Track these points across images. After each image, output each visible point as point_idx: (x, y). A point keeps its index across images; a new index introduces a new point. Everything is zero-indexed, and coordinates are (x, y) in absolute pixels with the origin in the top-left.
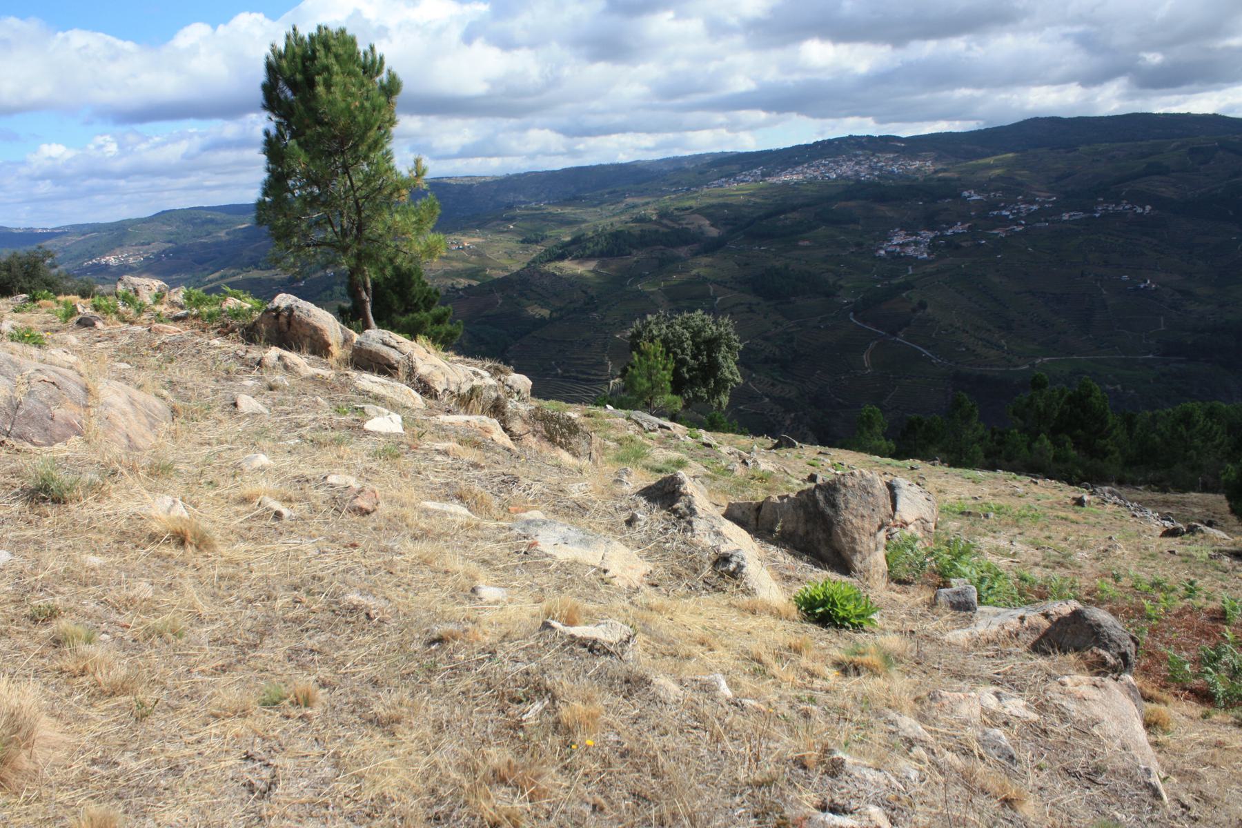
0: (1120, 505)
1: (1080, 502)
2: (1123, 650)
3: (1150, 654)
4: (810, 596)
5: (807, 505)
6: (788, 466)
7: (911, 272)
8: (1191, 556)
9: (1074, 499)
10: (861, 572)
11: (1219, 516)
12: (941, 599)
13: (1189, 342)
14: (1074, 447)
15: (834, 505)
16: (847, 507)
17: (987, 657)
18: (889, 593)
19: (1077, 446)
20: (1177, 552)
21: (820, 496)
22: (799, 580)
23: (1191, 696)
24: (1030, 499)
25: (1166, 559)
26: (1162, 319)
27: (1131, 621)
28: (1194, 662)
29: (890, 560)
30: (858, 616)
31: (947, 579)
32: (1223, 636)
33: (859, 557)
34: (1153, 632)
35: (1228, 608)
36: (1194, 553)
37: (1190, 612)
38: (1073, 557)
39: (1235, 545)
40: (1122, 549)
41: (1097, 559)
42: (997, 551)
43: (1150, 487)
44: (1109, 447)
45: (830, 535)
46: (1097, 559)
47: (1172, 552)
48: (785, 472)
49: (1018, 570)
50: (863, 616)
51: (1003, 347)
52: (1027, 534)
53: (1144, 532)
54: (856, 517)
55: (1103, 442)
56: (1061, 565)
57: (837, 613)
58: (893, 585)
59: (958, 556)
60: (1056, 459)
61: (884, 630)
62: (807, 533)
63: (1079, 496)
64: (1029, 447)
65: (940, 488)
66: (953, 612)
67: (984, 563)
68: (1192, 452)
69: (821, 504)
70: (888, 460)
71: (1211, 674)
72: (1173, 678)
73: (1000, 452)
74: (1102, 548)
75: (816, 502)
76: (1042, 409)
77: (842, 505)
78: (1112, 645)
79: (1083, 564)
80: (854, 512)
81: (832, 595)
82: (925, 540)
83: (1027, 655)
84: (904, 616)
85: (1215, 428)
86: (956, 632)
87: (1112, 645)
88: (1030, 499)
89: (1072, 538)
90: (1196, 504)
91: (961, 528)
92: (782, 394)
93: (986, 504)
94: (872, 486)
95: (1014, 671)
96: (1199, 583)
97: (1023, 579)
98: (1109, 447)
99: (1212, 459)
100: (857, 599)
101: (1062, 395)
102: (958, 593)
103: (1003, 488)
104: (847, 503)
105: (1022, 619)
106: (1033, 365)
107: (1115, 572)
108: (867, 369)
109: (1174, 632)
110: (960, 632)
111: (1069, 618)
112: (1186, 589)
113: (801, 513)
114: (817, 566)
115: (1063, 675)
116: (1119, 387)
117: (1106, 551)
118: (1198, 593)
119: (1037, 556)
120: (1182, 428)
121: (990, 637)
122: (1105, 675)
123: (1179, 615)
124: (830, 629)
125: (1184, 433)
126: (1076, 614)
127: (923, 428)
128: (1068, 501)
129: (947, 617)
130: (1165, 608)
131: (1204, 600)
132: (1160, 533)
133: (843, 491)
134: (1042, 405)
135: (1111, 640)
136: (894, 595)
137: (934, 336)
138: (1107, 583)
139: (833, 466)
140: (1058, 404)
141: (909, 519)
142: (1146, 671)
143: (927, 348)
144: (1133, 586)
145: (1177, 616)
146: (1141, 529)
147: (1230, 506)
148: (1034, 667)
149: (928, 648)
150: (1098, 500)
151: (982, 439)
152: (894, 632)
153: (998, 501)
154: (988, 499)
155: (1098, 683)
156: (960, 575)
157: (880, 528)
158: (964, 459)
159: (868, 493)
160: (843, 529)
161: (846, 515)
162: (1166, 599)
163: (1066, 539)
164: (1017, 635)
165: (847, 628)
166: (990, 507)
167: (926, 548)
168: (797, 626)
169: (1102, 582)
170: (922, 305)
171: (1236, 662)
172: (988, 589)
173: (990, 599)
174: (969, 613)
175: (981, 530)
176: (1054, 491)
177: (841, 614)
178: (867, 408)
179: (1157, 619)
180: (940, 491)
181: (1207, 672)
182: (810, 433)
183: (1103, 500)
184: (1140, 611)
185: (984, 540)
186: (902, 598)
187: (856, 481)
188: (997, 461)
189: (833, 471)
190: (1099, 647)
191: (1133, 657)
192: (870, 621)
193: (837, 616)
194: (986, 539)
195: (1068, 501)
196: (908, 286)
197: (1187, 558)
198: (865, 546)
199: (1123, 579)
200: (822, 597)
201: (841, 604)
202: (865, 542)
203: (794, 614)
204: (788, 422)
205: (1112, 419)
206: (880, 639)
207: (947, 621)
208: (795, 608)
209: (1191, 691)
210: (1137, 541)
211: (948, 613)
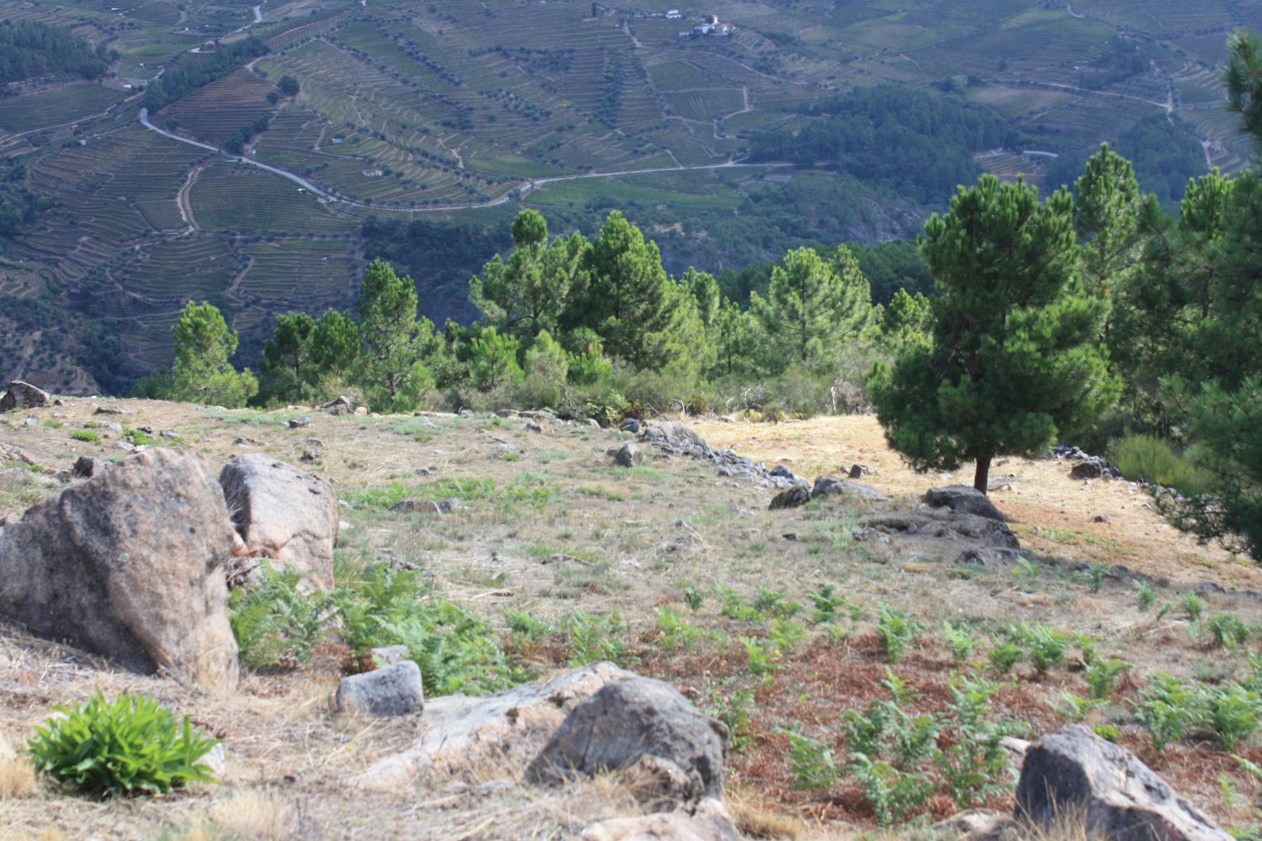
0: (695, 457)
1: (622, 458)
2: (699, 753)
3: (762, 742)
4: (63, 736)
5: (48, 536)
6: (32, 447)
7: (259, 19)
8: (823, 540)
9: (610, 453)
10: (179, 664)
11: (868, 456)
12: (350, 697)
13: (796, 134)
14: (605, 351)
15: (106, 530)
16: (134, 533)
17: (443, 808)
18: (243, 700)
19: (609, 350)
20: (798, 534)
21: (73, 515)
22: (45, 701)
23: (836, 810)
24: (528, 464)
25: (781, 551)
26: (745, 91)
27: (726, 682)
28: (840, 743)
29: (241, 629)
30: (169, 765)
31: (365, 651)
32: (884, 686)
33: (172, 633)
34: (763, 697)
35: (889, 633)
36: (828, 534)
37: (827, 648)
38: (612, 571)
39: (895, 508)
40: (703, 544)
41: (657, 568)
42: (468, 578)
43: (747, 414)
44: (668, 345)
45: (105, 593)
46: (657, 568)
47: (790, 537)
48: (25, 460)
49: (509, 611)
50: (181, 762)
51: (455, 163)
52: (524, 533)
53: (742, 502)
54: (156, 549)
55: (657, 336)
56: (590, 587)
57: (124, 765)
58: (254, 680)
59: (382, 603)
60: (573, 376)
61: (229, 784)
62: (55, 596)
63: (617, 446)
64: (521, 360)
65: (351, 459)
66: (377, 721)
67: (441, 605)
68: (814, 341)
69: (79, 531)
70: (243, 412)
71: (865, 765)
72: (804, 783)
73: (466, 374)
74: (665, 545)
75: (67, 528)
76: (538, 283)
77: (125, 529)
78: (678, 746)
79: (631, 581)
80: (152, 540)
81: (109, 729)
82: (315, 577)
83: (523, 791)
84: (278, 744)
85: (850, 292)
86: (385, 761)
87: (678, 746)
88: (528, 464)
89: (609, 533)
90: (829, 438)
91: (394, 537)
92: (11, 293)
93: (444, 480)
94: (185, 481)
95: (497, 830)
96: (838, 589)
97: (520, 627)
98: (668, 345)
99: (850, 350)
100: (164, 729)
101: (573, 253)
102: (382, 681)
103: (475, 446)
104: (133, 525)
105: (512, 715)
106: (516, 196)
107: (690, 591)
108: (186, 226)
109: (801, 692)
110: (394, 760)
111: (594, 706)
112: (818, 606)
113: (38, 555)
114: (82, 663)
115: (590, 822)
116: (678, 227)
117: (674, 549)
118: (838, 610)
119: (544, 577)
120: (793, 298)
121: (454, 763)
122: (671, 807)
123: (808, 657)
124: (112, 802)
125: (798, 303)
126: (608, 696)
127: (310, 339)
128: (600, 457)
129: (366, 732)
130: (782, 648)
131: (849, 622)
132: (768, 501)
133: (124, 497)
134: (537, 273)
135: (675, 738)
136: (256, 702)
137: (317, 148)
138: (677, 614)
139: (129, 436)
140: (567, 270)
141: (278, 536)
142: (756, 776)
143: (306, 175)
144: (724, 613)
145: (805, 659)
146: (736, 497)
147: (887, 435)
148: (532, 817)
149: (323, 810)
150: (654, 451)
151: (429, 349)
152: (253, 785)
153: (468, 473)
154: (449, 471)
155: (657, 828)
156: (389, 639)
157: (211, 566)
158: (398, 396)
159: (178, 495)
160: (131, 578)
161: (131, 548)
162: (783, 630)
163: (597, 536)
164: (506, 747)
165: (149, 794)
166: (453, 487)
167: (317, 593)
168: (39, 809)
169: (668, 611)
170: (289, 87)
171: (906, 733)
172: (446, 661)
173: (453, 680)
174: (410, 717)
175: (431, 537)
176: (573, 442)
177: (133, 765)
178: (192, 310)
179: (771, 671)
180: (354, 466)
181: (858, 762)
182: (79, 370)
183: (664, 449)
184: (740, 658)
185: (438, 558)
186: (272, 705)
187: (149, 473)
188: (462, 392)
189: (129, 447)
190: (655, 754)
191: (719, 762)
192: (198, 771)
193: (124, 773)
194: (445, 555)
195: (600, 457)
196: (255, 49)
197: (816, 547)
198: (183, 608)
199: (706, 602)
200: (88, 735)
201: (131, 745)
202: (182, 598)
203: (32, 783)
204: (30, 351)
205: (669, 290)
206: (220, 808)
207: (367, 741)
208: (30, 770)
209: (837, 802)
210: (727, 522)
211: (366, 724)
